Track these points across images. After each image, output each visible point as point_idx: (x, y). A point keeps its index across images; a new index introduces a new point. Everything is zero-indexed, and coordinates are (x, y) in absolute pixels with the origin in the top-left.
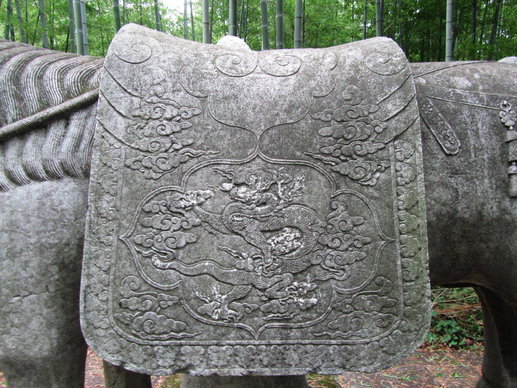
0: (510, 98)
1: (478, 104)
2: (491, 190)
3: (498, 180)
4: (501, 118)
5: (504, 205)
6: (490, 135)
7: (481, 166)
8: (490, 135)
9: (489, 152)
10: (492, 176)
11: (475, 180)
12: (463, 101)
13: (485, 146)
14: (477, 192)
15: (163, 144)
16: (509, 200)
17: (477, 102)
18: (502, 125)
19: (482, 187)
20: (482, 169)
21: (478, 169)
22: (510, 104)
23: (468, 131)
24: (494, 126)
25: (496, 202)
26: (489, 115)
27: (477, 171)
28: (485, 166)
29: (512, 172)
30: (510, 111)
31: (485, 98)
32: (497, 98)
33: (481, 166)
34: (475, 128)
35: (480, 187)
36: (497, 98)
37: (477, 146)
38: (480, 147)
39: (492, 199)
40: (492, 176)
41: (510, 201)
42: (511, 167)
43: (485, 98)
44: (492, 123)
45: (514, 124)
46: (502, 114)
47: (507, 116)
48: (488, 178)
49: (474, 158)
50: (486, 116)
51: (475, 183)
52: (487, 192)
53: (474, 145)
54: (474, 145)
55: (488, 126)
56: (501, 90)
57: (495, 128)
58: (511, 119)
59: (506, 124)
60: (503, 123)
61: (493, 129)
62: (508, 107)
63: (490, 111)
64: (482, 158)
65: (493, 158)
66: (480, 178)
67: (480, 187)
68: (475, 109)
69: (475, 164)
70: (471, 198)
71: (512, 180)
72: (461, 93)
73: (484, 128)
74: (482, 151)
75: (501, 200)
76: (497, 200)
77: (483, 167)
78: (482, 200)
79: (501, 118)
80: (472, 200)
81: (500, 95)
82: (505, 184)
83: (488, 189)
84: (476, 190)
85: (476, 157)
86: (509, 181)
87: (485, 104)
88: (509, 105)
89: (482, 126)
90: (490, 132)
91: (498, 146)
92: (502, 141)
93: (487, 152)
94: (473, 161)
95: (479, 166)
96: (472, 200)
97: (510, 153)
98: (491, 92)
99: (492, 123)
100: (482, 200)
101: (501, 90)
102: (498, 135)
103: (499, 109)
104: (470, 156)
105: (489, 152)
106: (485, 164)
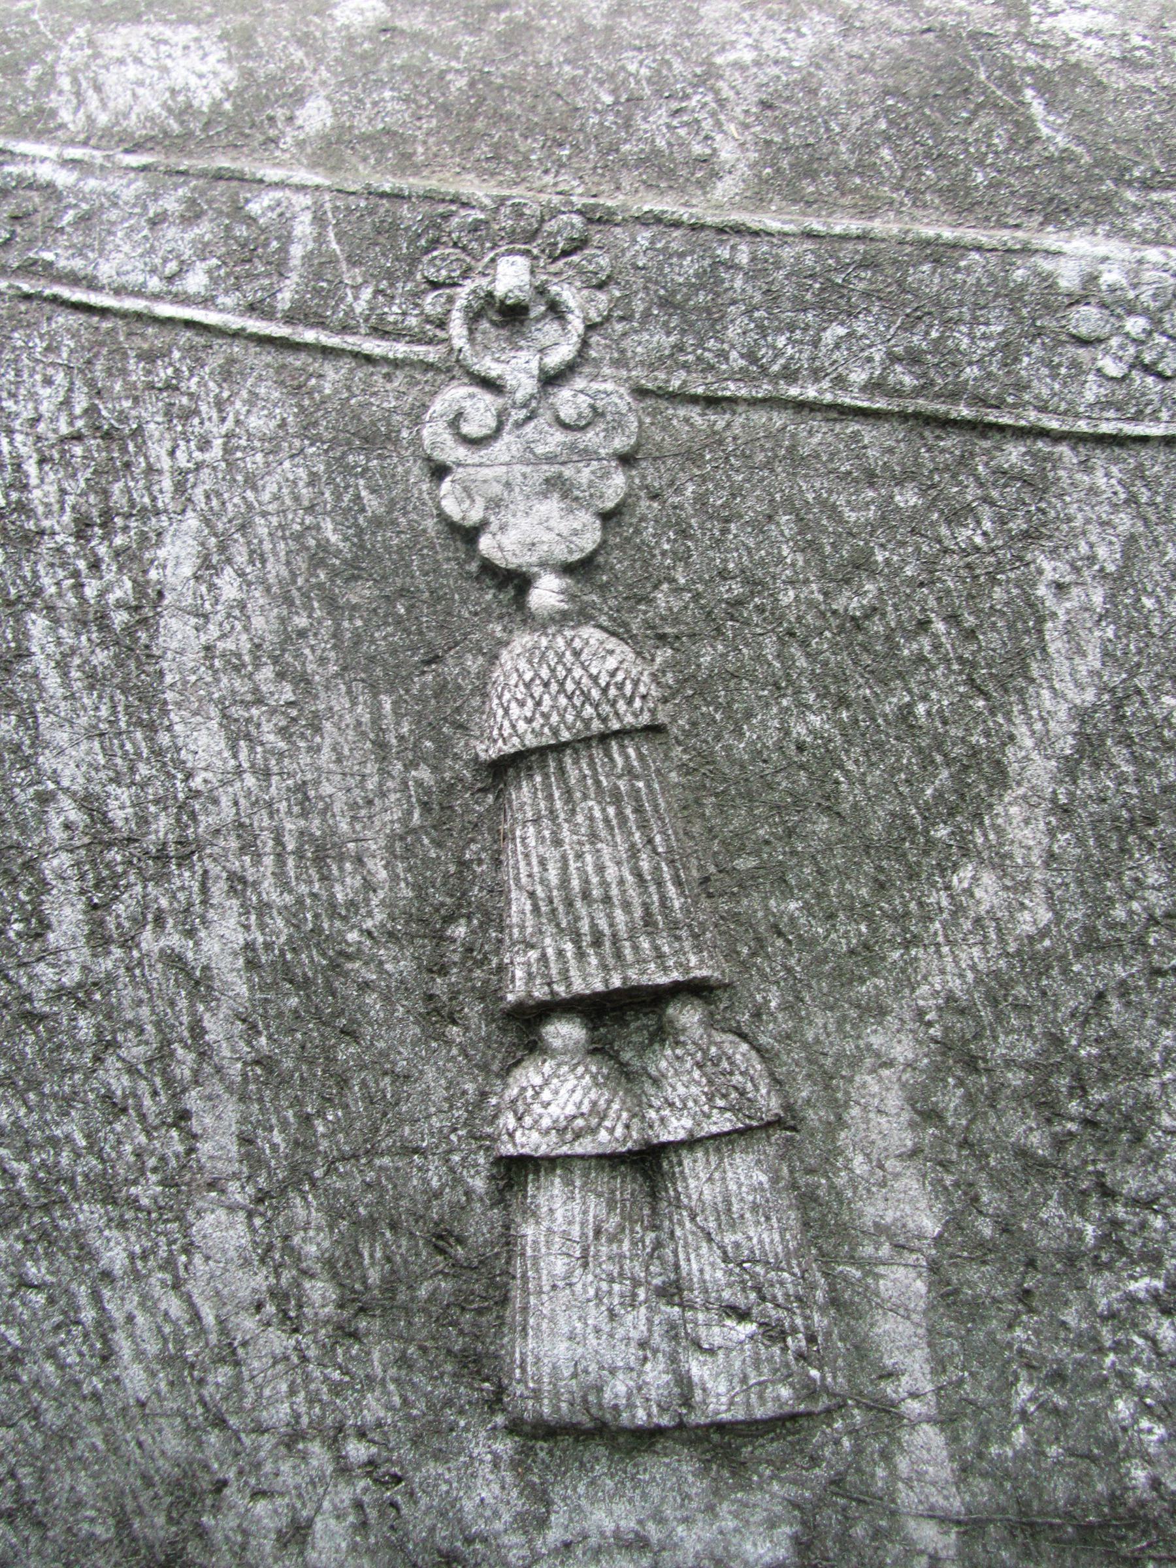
0: (598, 218)
1: (207, 301)
2: (278, 1341)
3: (370, 1225)
4: (439, 471)
5: (448, 1511)
6: (303, 681)
7: (163, 1055)
8: (303, 681)
9: (270, 891)
10: (299, 1176)
11: (89, 1213)
12: (48, 271)
13: (227, 812)
14: (107, 1356)
15: (1005, 486)
16: (505, 1446)
17: (196, 281)
18: (448, 559)
19: (173, 1305)
20: (176, 1090)
21: (120, 1084)
22: (569, 295)
23: (37, 625)
24: (353, 572)
25: (344, 1469)
26: (307, 428)
27: (115, 1107)
28: (204, 1054)
29: (530, 1142)
30: (551, 380)
31: (303, 227)
32: (436, 223)
33: (163, 1055)
34: (124, 590)
35: (147, 1302)
36: (436, 223)
37: (120, 812)
38: (162, 825)
39: (293, 1438)
40: (299, 1176)
41: (520, 1464)
42: (529, 1075)
43: (303, 227)
44: (330, 532)
45: (589, 540)
46: (456, 421)
47: (501, 449)
48: (238, 1193)
49: (80, 954)
50: (273, 445)
51: (88, 1254)
52: (229, 1354)
53: (90, 803)
54: (90, 803)
55: (275, 569)
56: (534, 147)
57: (361, 593)
58: (557, 486)
59: (485, 544)
60: (469, 535)
61: (332, 604)
62: (550, 330)
63: (332, 375)
64: (174, 960)
65: (309, 961)
66: (147, 1191)
67: (147, 1302)
68: (149, 357)
69: (85, 1026)
70: (52, 1417)
71: (529, 1230)
72: (64, 178)
73: (229, 586)
74: (186, 879)
75: (407, 1453)
76: (357, 1451)
77: (185, 1060)
78: (173, 1443)
79: (439, 471)
80: (63, 1437)
81: (480, 190)
82: (458, 1269)
83: (248, 1323)
84: (104, 1327)
85: (99, 940)
86: (508, 1240)
87: (285, 299)
88: (556, 310)
89: (207, 568)
90: (290, 638)
91: (390, 816)
92: (444, 747)
93: (237, 883)
94: (59, 993)
95: (136, 1051)
96: (63, 1437)
97: (519, 905)
98: (406, 163)
99: (330, 532)
100: (173, 1443)
101: (534, 147)
102: (397, 680)
103: (432, 354)
104: (39, 928)
105: (270, 891)
106: (215, 1029)
